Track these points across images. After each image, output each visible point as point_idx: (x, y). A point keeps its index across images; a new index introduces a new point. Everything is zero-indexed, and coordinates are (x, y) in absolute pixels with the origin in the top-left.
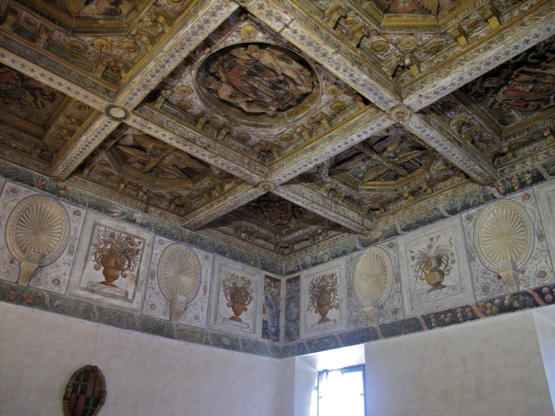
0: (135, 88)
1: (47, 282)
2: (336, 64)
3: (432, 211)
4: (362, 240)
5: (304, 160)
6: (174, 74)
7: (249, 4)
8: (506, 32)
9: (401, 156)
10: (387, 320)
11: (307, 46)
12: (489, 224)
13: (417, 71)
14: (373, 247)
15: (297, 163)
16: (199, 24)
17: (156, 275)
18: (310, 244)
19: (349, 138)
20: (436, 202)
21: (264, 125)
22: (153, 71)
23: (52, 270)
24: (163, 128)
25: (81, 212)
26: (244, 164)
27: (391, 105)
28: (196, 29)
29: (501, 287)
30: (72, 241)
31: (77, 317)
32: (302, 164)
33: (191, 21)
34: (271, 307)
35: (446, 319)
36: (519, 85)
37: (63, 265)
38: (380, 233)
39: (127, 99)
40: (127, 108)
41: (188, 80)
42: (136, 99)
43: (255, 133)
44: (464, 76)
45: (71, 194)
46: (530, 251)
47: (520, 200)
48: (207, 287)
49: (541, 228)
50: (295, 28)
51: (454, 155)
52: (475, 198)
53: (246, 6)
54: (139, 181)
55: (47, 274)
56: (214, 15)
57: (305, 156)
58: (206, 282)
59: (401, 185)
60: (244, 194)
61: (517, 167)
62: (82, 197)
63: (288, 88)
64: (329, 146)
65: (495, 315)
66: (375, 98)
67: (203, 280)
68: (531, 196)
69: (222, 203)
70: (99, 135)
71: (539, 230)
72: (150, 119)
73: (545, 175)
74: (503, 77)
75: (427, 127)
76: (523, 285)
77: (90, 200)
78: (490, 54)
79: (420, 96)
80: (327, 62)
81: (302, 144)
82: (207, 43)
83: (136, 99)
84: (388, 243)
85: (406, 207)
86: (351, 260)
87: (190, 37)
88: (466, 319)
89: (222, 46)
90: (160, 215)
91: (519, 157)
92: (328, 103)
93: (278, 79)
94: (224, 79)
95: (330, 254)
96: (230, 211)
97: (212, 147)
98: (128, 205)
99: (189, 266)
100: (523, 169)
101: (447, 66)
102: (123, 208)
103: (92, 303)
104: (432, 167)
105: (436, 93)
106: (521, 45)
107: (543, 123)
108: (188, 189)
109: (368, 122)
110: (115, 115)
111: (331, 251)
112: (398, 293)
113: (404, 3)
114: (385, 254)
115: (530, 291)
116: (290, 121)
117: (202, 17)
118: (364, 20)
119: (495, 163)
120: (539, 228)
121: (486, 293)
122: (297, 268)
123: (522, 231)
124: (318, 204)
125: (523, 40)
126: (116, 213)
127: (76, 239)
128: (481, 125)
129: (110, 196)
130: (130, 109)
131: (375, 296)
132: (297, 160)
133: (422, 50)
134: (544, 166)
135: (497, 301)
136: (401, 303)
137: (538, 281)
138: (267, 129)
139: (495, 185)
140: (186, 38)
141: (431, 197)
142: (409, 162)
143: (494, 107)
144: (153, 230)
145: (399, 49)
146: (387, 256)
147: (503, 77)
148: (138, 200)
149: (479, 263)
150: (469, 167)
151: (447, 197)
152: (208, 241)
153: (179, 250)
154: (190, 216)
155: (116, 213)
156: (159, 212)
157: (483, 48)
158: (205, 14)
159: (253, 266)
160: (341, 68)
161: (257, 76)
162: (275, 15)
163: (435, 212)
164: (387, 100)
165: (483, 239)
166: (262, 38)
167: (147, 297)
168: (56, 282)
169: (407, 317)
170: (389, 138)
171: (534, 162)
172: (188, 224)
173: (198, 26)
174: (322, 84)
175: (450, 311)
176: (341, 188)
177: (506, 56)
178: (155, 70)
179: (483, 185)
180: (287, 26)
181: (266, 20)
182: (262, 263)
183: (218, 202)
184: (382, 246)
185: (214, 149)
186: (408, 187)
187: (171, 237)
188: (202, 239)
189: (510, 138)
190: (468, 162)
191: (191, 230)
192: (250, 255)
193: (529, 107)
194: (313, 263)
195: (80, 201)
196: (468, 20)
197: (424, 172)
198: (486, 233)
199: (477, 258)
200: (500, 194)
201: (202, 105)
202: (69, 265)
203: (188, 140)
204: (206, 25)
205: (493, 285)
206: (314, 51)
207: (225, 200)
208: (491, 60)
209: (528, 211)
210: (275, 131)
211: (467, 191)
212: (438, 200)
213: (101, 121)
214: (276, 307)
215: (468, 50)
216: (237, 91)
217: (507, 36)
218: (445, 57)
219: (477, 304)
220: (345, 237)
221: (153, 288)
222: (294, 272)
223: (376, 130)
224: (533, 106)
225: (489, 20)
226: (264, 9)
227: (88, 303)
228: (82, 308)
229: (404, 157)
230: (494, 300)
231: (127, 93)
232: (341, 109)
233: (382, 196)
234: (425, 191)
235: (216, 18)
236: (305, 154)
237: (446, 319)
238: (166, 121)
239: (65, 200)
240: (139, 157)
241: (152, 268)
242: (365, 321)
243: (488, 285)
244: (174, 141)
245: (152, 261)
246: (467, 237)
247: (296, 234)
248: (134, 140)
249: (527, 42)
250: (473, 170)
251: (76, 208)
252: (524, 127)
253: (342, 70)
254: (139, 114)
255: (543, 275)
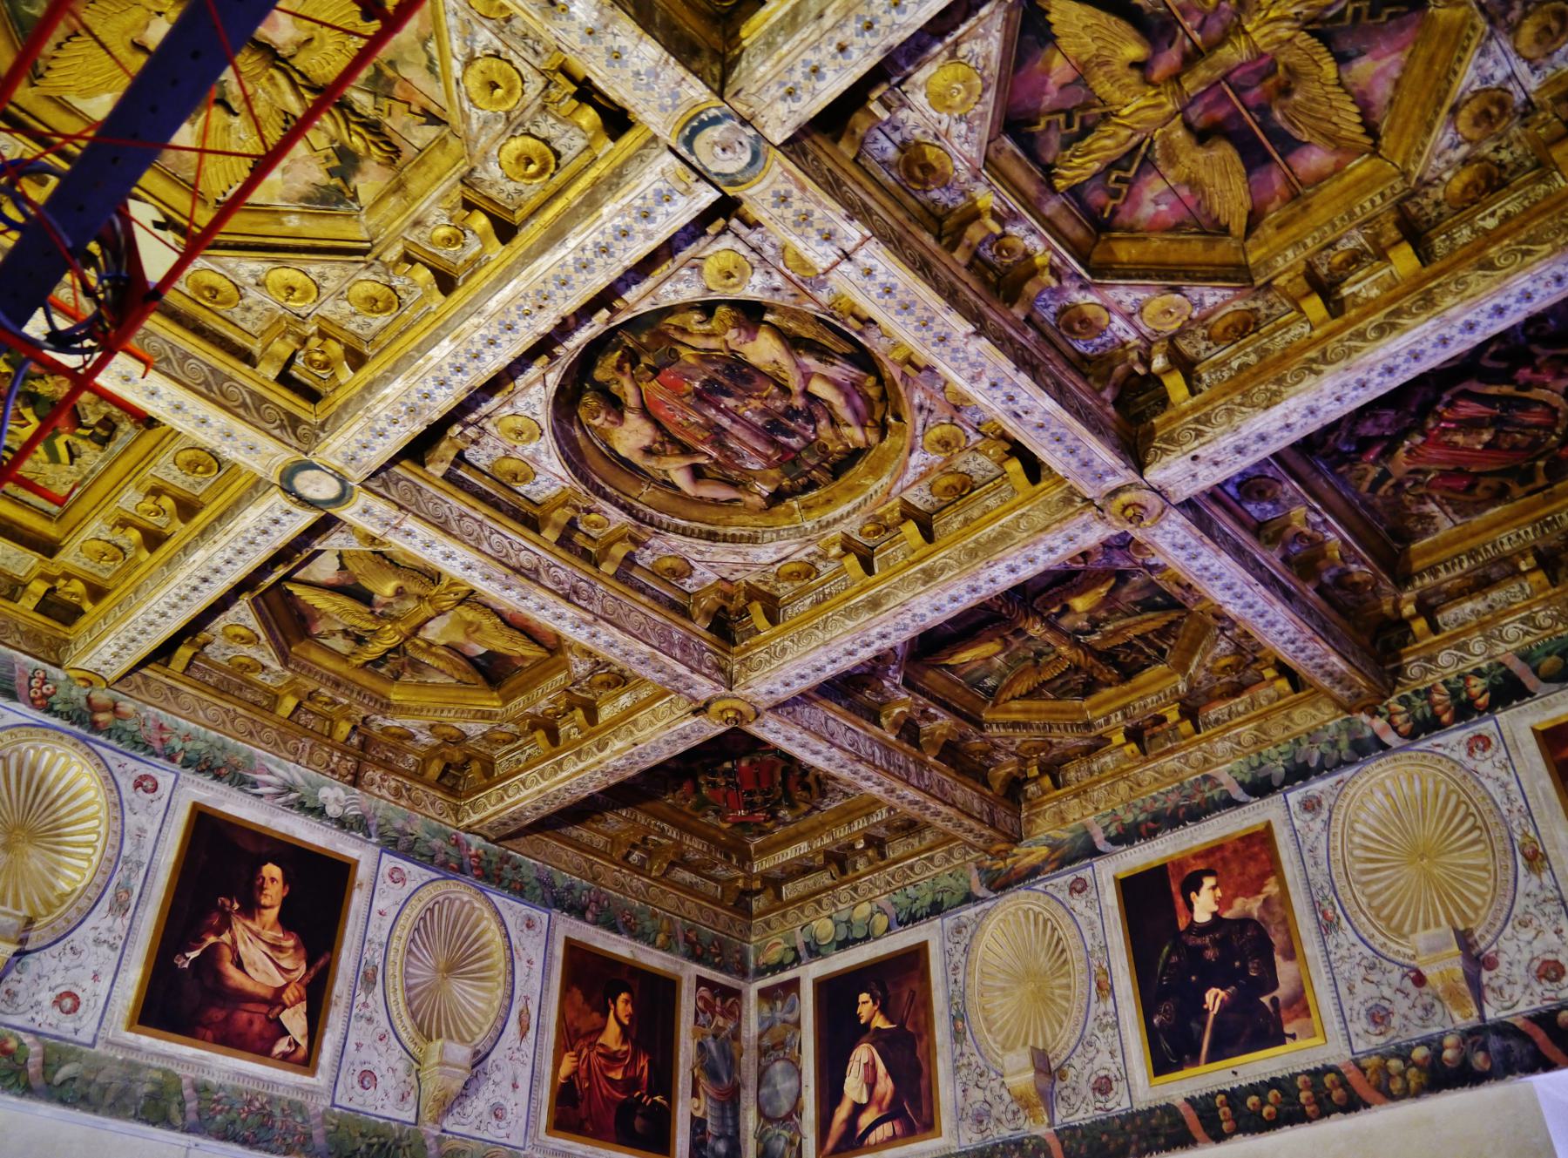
0: (382, 415)
1: (38, 1003)
2: (972, 365)
3: (1196, 785)
4: (989, 870)
5: (848, 637)
6: (495, 384)
7: (749, 192)
8: (1439, 285)
9: (1110, 627)
10: (1081, 1115)
11: (898, 313)
12: (1371, 821)
13: (1185, 391)
14: (1023, 892)
15: (826, 644)
16: (600, 239)
17: (379, 977)
18: (829, 882)
19: (985, 576)
20: (1206, 760)
21: (733, 535)
22: (446, 367)
23: (55, 962)
24: (448, 533)
25: (160, 780)
26: (672, 645)
27: (1112, 482)
28: (589, 254)
29: (1428, 1009)
30: (126, 873)
31: (127, 1118)
32: (841, 649)
33: (578, 229)
34: (714, 1076)
35: (1266, 1111)
36: (1456, 431)
37: (93, 949)
38: (1044, 851)
39: (354, 446)
40: (349, 472)
41: (534, 400)
42: (379, 449)
43: (707, 557)
44: (1320, 404)
45: (131, 725)
46: (1507, 902)
47: (1461, 754)
48: (528, 1014)
49: (1532, 833)
50: (870, 262)
51: (1272, 624)
52: (1325, 748)
53: (740, 195)
54: (342, 689)
55: (40, 977)
56: (646, 215)
57: (850, 624)
58: (527, 998)
59: (1102, 711)
60: (660, 734)
61: (1444, 658)
62: (165, 736)
63: (815, 431)
64: (924, 598)
65: (1417, 1095)
66: (1068, 464)
67: (517, 993)
68: (1493, 741)
69: (591, 760)
70: (249, 548)
71: (1527, 840)
72: (414, 508)
73: (1530, 680)
74: (1413, 409)
75: (1204, 544)
76: (1496, 1004)
77: (189, 745)
78: (1395, 345)
79: (1195, 458)
80: (947, 359)
81: (838, 593)
82: (606, 298)
83: (379, 449)
84: (1069, 878)
85: (1120, 774)
86: (958, 930)
87: (569, 277)
88: (1325, 1108)
89: (645, 307)
90: (397, 793)
91: (1448, 631)
92: (923, 476)
93: (790, 407)
94: (632, 400)
95: (892, 911)
96: (612, 782)
97: (585, 595)
98: (303, 761)
99: (478, 950)
100: (1461, 666)
101: (1271, 376)
102: (287, 770)
103: (179, 1071)
104: (1196, 659)
105: (1240, 450)
106: (1484, 320)
107: (1513, 537)
108: (487, 716)
109: (1041, 531)
110: (310, 493)
111: (894, 904)
112: (1109, 1031)
113: (1157, 203)
114: (1061, 911)
115: (1520, 1023)
116: (808, 525)
117: (611, 219)
118: (1049, 248)
119: (1378, 647)
120: (1525, 834)
121: (1382, 1028)
122: (790, 956)
123: (1474, 842)
124: (873, 763)
125: (1488, 306)
126: (269, 785)
127: (139, 864)
128: (1344, 541)
129: (251, 734)
130: (356, 476)
131: (1035, 1039)
132: (828, 637)
133: (1201, 332)
134: (1525, 656)
135: (1419, 1053)
136: (1119, 1059)
137: (1538, 989)
138: (743, 547)
139: (1382, 709)
140: (556, 277)
141: (1190, 745)
142: (1129, 645)
143: (1381, 492)
144: (374, 840)
145: (1137, 329)
146: (1068, 920)
147: (1413, 409)
148: (334, 747)
149: (1353, 938)
150: (1311, 658)
151: (1239, 743)
152: (534, 874)
153: (452, 902)
154: (487, 797)
155: (269, 785)
156: (393, 784)
157: (1376, 327)
158: (621, 213)
159: (662, 948)
160: (984, 379)
161: (729, 394)
162: (817, 225)
163: (1206, 787)
164: (1101, 470)
165: (1358, 866)
166: (763, 290)
167: (351, 1046)
168: (68, 1003)
169: (1140, 1105)
170: (1080, 578)
171: (1492, 645)
172: (481, 821)
173: (596, 244)
174: (914, 422)
175: (1274, 1083)
176: (936, 717)
177: (1440, 349)
178: (451, 365)
179: (1349, 711)
180: (847, 256)
181: (793, 238)
182: (686, 939)
183: (578, 754)
184: (1050, 889)
185: (590, 599)
186: (1125, 716)
187: (427, 860)
188: (517, 867)
189: (1422, 577)
190: (1311, 645)
191: (486, 839)
192: (655, 915)
193: (1478, 491)
194: (840, 938)
195: (157, 745)
196: (1332, 252)
197: (1171, 675)
198: (1366, 848)
199: (1344, 922)
200: (1400, 735)
201: (563, 473)
202: (113, 947)
203: (517, 571)
204: (620, 245)
205: (1401, 1005)
206: (917, 329)
207: (601, 750)
208: (1399, 360)
209: (1489, 784)
210: (765, 554)
211: (1299, 729)
212: (1213, 753)
213: (264, 508)
214: (729, 1078)
215: (1330, 335)
216: (668, 441)
217: (1443, 295)
218: (1262, 353)
219: (1356, 1062)
220: (937, 862)
221: (370, 1020)
222: (781, 966)
223: (1061, 552)
224: (1487, 488)
225: (1391, 254)
226: (789, 206)
227: (166, 1072)
228: (147, 1088)
229: (1115, 632)
230: (1410, 1048)
231: (356, 428)
232: (963, 489)
233: (1050, 743)
234: (1175, 727)
235: (651, 227)
236: (850, 619)
237: (1266, 1111)
238: (456, 513)
239: (112, 743)
240: (349, 621)
241: (367, 956)
242: (1010, 1116)
243: (1385, 1004)
244: (476, 574)
245: (369, 935)
246: (1309, 861)
247: (789, 853)
248: (343, 567)
249: (1500, 311)
250: (1321, 667)
251: (143, 769)
252: (1457, 548)
253: (985, 383)
254: (382, 490)
255: (1553, 974)
